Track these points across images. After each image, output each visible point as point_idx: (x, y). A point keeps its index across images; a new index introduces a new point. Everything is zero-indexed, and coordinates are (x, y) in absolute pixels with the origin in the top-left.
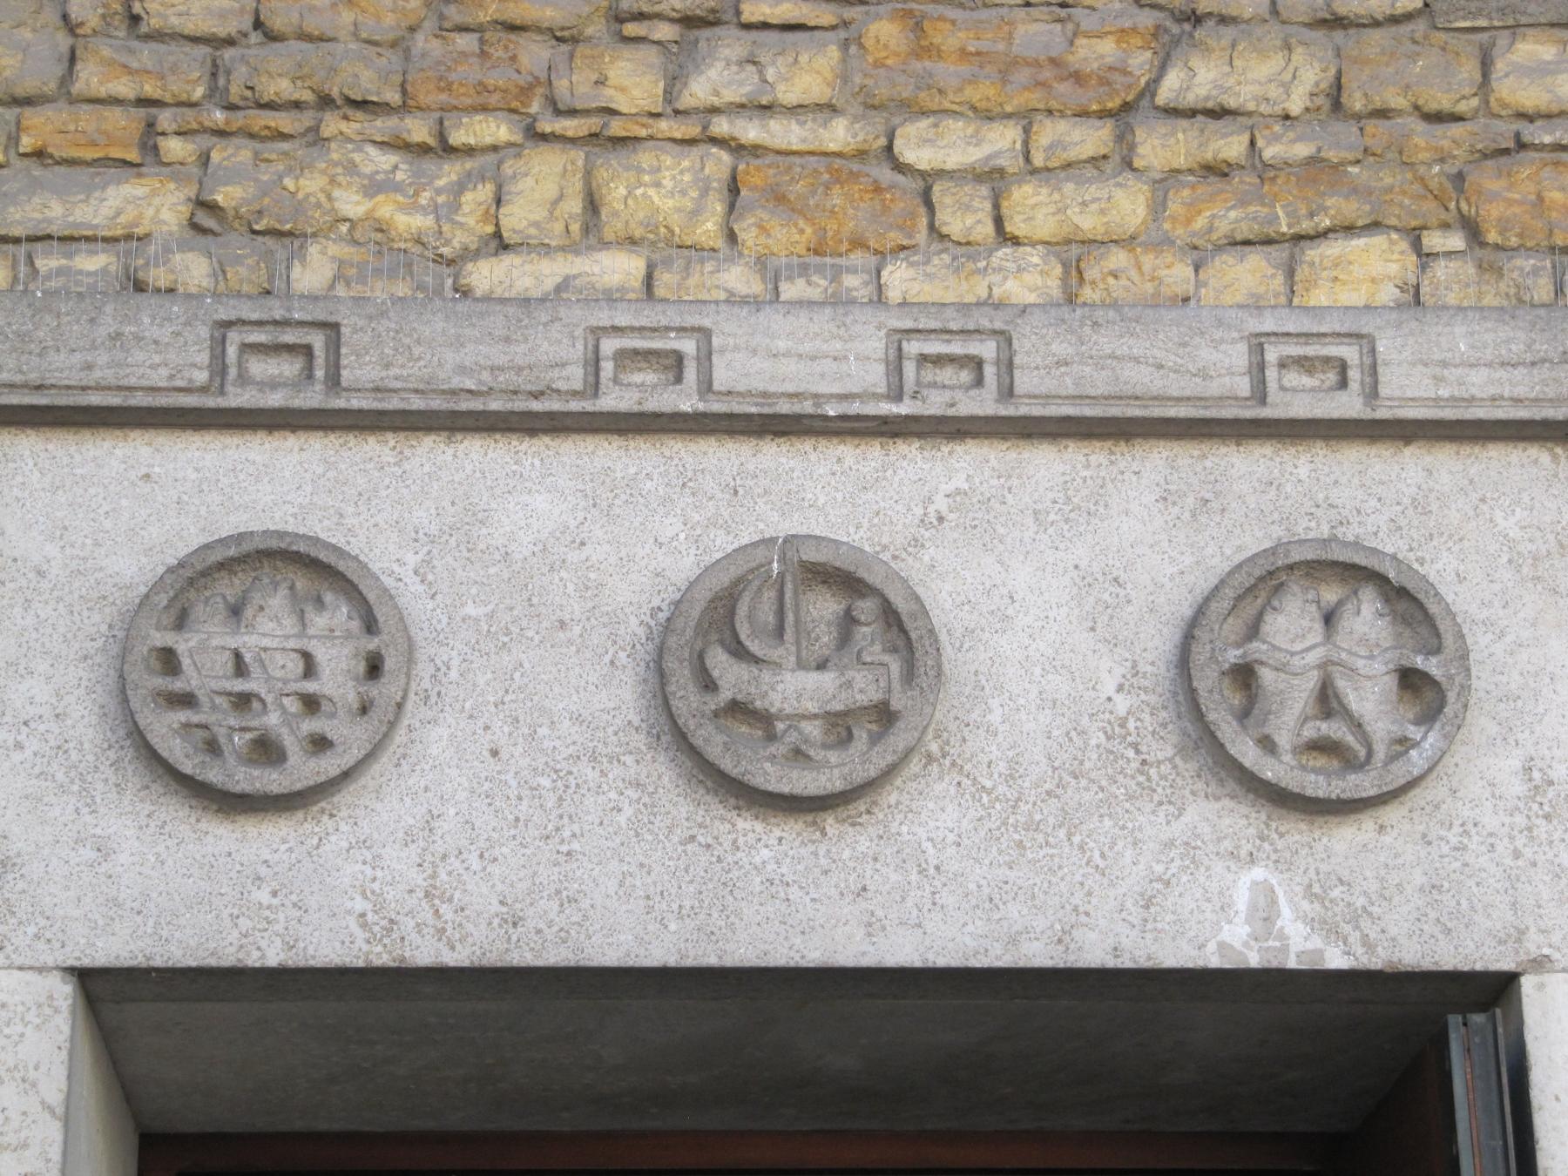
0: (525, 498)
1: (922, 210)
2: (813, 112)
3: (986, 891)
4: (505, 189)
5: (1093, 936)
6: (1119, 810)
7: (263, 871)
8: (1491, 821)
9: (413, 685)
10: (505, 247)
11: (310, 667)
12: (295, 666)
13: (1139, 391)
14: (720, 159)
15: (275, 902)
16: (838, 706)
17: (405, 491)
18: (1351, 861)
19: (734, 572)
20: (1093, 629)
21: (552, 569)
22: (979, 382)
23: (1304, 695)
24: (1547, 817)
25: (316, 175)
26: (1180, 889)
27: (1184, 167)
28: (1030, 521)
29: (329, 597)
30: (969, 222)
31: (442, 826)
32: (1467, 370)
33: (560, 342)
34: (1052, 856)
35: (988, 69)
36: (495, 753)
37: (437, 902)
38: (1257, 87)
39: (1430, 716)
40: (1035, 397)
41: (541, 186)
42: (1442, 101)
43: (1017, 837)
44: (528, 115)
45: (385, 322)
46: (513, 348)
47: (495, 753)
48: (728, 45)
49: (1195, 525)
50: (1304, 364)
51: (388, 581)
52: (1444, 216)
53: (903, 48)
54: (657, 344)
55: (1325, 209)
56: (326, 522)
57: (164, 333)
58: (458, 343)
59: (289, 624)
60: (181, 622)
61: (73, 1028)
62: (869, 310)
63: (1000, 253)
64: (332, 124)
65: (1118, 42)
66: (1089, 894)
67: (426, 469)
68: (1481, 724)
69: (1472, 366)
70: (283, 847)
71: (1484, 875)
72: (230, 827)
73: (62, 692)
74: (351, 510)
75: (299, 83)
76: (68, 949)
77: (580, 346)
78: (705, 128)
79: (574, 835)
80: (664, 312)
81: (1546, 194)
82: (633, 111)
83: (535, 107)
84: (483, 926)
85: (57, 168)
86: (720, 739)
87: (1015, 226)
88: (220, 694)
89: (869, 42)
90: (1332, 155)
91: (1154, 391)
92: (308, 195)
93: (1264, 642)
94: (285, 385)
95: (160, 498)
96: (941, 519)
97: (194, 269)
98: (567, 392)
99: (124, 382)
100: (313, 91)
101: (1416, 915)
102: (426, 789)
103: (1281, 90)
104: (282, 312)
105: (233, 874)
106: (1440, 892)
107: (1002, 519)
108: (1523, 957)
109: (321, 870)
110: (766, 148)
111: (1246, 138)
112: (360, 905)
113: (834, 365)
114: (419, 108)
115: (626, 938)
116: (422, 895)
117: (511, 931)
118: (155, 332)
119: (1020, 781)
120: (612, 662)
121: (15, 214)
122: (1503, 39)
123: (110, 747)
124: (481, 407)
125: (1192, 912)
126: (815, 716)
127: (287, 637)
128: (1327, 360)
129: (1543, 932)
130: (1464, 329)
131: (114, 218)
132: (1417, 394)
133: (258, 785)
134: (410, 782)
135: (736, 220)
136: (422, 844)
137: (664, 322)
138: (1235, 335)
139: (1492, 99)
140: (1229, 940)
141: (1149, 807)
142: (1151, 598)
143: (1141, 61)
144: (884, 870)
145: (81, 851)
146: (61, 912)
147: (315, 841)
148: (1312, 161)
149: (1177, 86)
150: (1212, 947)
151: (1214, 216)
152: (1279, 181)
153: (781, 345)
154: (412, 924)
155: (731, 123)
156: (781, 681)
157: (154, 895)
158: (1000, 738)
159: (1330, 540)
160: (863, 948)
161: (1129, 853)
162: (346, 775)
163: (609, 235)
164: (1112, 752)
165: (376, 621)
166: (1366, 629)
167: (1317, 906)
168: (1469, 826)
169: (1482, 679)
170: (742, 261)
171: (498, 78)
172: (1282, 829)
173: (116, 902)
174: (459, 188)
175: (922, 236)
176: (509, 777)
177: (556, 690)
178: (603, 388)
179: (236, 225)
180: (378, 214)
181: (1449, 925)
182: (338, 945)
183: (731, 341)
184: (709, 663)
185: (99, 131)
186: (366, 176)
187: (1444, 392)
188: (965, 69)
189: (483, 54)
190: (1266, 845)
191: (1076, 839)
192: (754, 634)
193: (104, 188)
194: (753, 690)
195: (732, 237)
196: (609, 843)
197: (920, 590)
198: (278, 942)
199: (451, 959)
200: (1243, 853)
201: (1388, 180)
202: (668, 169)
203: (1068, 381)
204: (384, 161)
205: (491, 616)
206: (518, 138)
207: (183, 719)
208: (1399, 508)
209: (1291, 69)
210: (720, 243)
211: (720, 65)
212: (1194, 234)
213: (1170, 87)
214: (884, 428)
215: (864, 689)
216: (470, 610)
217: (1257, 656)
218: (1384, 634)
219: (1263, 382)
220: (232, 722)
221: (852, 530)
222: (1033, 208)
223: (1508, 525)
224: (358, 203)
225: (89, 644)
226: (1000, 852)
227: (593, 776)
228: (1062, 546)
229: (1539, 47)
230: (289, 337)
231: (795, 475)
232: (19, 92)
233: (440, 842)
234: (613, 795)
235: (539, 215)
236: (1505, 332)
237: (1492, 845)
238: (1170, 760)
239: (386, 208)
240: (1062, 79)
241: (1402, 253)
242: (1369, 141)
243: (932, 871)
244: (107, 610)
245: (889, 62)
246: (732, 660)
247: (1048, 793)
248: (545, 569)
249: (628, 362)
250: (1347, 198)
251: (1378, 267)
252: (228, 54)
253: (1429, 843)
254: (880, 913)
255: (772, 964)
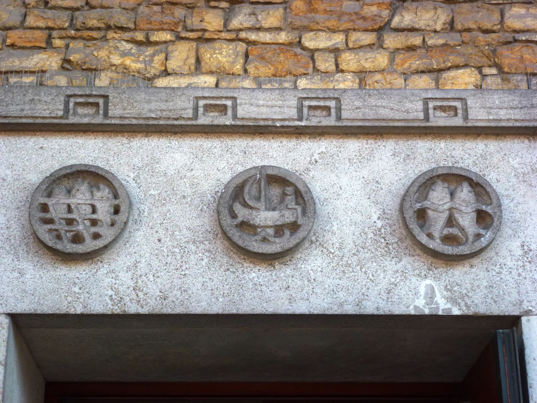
0: (172, 155)
1: (311, 62)
2: (274, 30)
3: (332, 287)
4: (169, 55)
5: (369, 303)
6: (379, 260)
7: (77, 281)
8: (510, 264)
9: (131, 218)
10: (169, 74)
11: (94, 210)
12: (89, 209)
13: (385, 117)
14: (242, 46)
15: (80, 291)
16: (279, 223)
17: (131, 152)
18: (461, 277)
19: (243, 178)
20: (369, 198)
21: (181, 178)
22: (329, 115)
23: (444, 219)
24: (530, 262)
25: (104, 50)
26: (399, 288)
27: (401, 48)
28: (347, 162)
29: (102, 186)
30: (327, 65)
31: (140, 265)
32: (499, 110)
33: (184, 101)
34: (355, 276)
35: (334, 16)
36: (159, 240)
37: (137, 291)
38: (425, 21)
39: (486, 228)
40: (349, 119)
41: (181, 55)
42: (487, 25)
43: (342, 269)
44: (177, 32)
45: (124, 95)
46: (168, 104)
47: (159, 240)
48: (245, 9)
49: (405, 163)
50: (443, 109)
51: (124, 182)
52: (490, 63)
53: (305, 10)
54: (218, 102)
55: (449, 60)
56: (103, 163)
57: (48, 99)
58: (149, 102)
59: (88, 195)
60: (50, 195)
61: (9, 334)
62: (292, 91)
63: (337, 75)
64: (111, 34)
65: (378, 7)
66: (368, 289)
67: (138, 145)
68: (507, 231)
69: (500, 109)
70: (84, 273)
71: (508, 282)
72: (66, 266)
73: (10, 220)
74: (112, 159)
75: (100, 21)
76: (8, 307)
77: (192, 103)
78: (237, 36)
79: (187, 268)
80: (221, 92)
81: (525, 56)
82: (213, 30)
83: (180, 29)
84: (154, 300)
85: (18, 50)
86: (238, 234)
87: (343, 66)
88: (62, 219)
89: (293, 7)
90: (451, 43)
91: (390, 117)
92: (102, 57)
93: (429, 201)
94: (89, 116)
95: (46, 155)
96: (316, 162)
97: (62, 80)
98: (187, 118)
99: (34, 115)
100: (105, 24)
101: (484, 296)
102: (135, 253)
103: (433, 22)
104: (89, 92)
105: (66, 282)
106: (493, 288)
107: (338, 162)
108: (522, 310)
109: (97, 280)
110: (258, 42)
111: (422, 38)
112: (110, 292)
113: (279, 109)
114: (140, 30)
115: (204, 304)
116: (132, 289)
117: (163, 301)
118: (46, 99)
119: (343, 250)
120: (201, 210)
121: (3, 64)
122: (507, 7)
123: (25, 238)
124: (157, 123)
125: (405, 295)
126: (271, 227)
127: (87, 200)
128: (450, 107)
129: (529, 302)
130: (497, 96)
131: (36, 65)
132: (482, 118)
133: (74, 250)
134: (129, 250)
135: (247, 65)
136: (133, 271)
137: (220, 95)
138: (418, 98)
139: (505, 26)
140: (418, 305)
141: (389, 259)
142: (390, 188)
143: (385, 13)
144: (295, 280)
145: (14, 274)
146: (6, 294)
147: (95, 271)
148: (445, 45)
149: (398, 21)
150: (412, 307)
151: (411, 63)
152: (433, 51)
153: (261, 102)
154: (128, 299)
155: (246, 34)
156: (262, 217)
157: (38, 289)
158: (337, 235)
159: (452, 167)
160: (288, 307)
161: (382, 275)
162: (106, 247)
163: (204, 70)
164: (376, 240)
165: (118, 194)
166: (465, 197)
167: (449, 293)
168: (503, 265)
169: (506, 215)
170: (249, 78)
171: (167, 19)
172: (436, 267)
173: (24, 291)
174: (153, 55)
175: (310, 70)
176: (164, 249)
177: (182, 219)
178: (199, 117)
179: (77, 67)
180: (125, 63)
181: (496, 299)
182: (102, 306)
183: (244, 101)
184: (234, 208)
185: (33, 38)
186: (121, 51)
187: (491, 117)
188: (326, 16)
189: (163, 12)
190: (431, 272)
191: (363, 270)
192: (250, 199)
193: (33, 55)
194: (250, 218)
195: (246, 71)
196: (199, 271)
197: (309, 185)
198: (81, 305)
199: (142, 311)
200: (423, 275)
201: (470, 51)
202: (224, 49)
203: (360, 114)
204: (128, 46)
205: (159, 194)
206: (173, 39)
207: (49, 228)
208: (476, 157)
209: (437, 15)
210: (242, 73)
211: (243, 15)
212: (404, 69)
213: (396, 21)
214: (297, 131)
215: (288, 217)
216: (152, 192)
217: (427, 206)
218: (472, 198)
219: (428, 114)
220: (66, 229)
221: (285, 165)
222: (349, 60)
223: (514, 163)
224: (119, 59)
225: (19, 204)
226: (337, 274)
227: (193, 248)
228: (358, 170)
229: (520, 10)
230: (91, 100)
231: (266, 147)
232: (7, 25)
233: (139, 271)
234: (201, 255)
235: (180, 64)
236: (511, 97)
237: (511, 272)
238: (396, 243)
239: (128, 62)
240: (359, 19)
241: (476, 74)
242: (464, 39)
243: (312, 281)
244: (26, 192)
245: (300, 14)
246: (242, 207)
247: (354, 254)
248: (179, 178)
249: (208, 109)
250: (456, 57)
251: (467, 79)
252: (77, 13)
253: (489, 271)
254: (294, 295)
255: (256, 313)
